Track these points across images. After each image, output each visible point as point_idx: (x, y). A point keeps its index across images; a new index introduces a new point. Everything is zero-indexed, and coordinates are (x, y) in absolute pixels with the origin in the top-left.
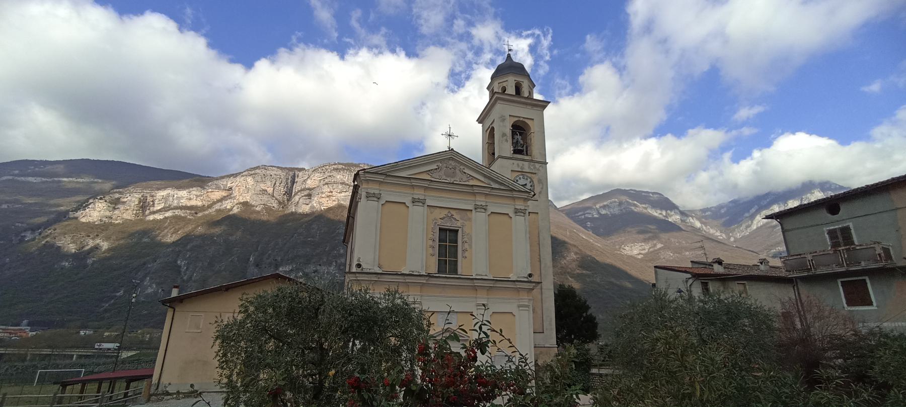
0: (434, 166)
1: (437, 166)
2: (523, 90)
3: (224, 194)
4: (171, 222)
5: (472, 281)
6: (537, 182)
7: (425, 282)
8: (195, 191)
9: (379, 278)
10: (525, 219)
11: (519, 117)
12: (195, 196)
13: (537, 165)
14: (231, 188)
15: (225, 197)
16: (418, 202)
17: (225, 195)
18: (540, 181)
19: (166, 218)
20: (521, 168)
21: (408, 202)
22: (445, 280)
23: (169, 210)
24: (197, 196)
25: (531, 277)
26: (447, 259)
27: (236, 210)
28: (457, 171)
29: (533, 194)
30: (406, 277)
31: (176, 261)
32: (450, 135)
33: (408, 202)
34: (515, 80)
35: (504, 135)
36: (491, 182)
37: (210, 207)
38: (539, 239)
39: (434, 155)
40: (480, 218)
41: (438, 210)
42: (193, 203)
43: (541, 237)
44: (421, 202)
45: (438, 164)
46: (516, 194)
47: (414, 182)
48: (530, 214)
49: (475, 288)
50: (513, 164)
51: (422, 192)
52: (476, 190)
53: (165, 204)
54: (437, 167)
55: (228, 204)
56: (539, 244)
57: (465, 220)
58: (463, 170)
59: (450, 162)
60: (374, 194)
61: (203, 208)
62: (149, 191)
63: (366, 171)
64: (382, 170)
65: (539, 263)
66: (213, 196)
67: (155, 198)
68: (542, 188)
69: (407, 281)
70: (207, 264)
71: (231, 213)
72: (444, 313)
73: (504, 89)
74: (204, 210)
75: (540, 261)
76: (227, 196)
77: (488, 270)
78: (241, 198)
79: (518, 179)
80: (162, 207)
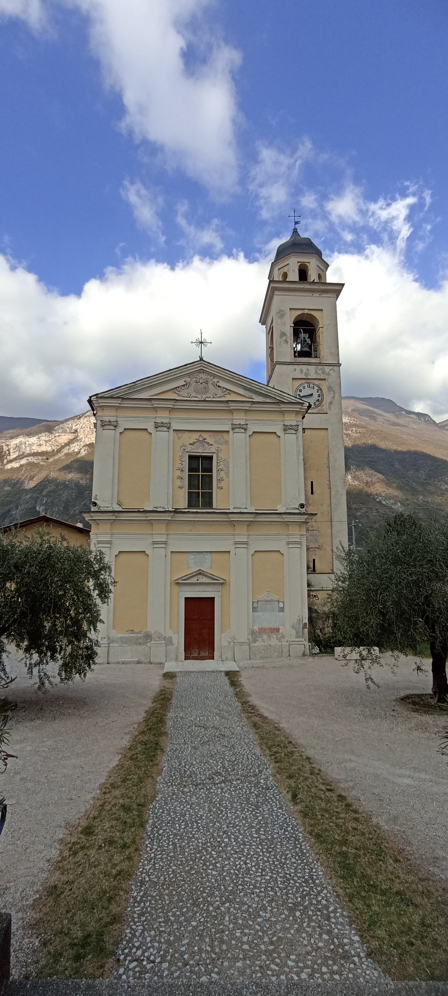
0: (181, 382)
1: (185, 381)
2: (309, 274)
3: (71, 436)
4: (26, 470)
5: (280, 516)
6: (327, 390)
7: (170, 519)
8: (44, 437)
9: (116, 517)
10: (297, 438)
11: (304, 309)
12: (44, 442)
13: (327, 369)
14: (76, 431)
15: (72, 440)
16: (162, 426)
17: (72, 438)
18: (330, 388)
19: (21, 466)
20: (305, 375)
21: (151, 429)
22: (195, 515)
23: (23, 458)
24: (46, 442)
25: (303, 507)
26: (200, 491)
27: (83, 453)
28: (210, 385)
29: (307, 405)
30: (147, 515)
31: (35, 508)
32: (201, 343)
33: (151, 429)
34: (298, 262)
35: (283, 334)
36: (252, 394)
37: (59, 451)
38: (329, 461)
39: (180, 369)
40: (239, 438)
41: (187, 435)
42: (44, 448)
43: (331, 459)
44: (166, 426)
45: (186, 379)
46: (284, 407)
47: (232, 406)
48: (306, 430)
49: (232, 524)
50: (295, 370)
51: (166, 414)
52: (233, 406)
53: (19, 452)
54: (185, 383)
55: (75, 447)
56: (329, 467)
57: (221, 444)
58: (218, 384)
59: (201, 375)
60: (240, 424)
61: (53, 453)
62: (3, 441)
63: (99, 396)
64: (118, 394)
65: (329, 490)
66: (60, 440)
67: (10, 447)
68: (334, 397)
69: (149, 518)
70: (62, 508)
71: (79, 456)
72: (196, 554)
73: (285, 275)
74: (54, 455)
75: (330, 488)
76: (74, 439)
77: (249, 502)
78: (87, 439)
79: (301, 388)
80: (17, 455)
